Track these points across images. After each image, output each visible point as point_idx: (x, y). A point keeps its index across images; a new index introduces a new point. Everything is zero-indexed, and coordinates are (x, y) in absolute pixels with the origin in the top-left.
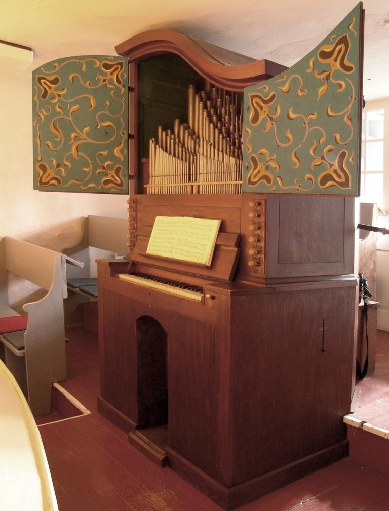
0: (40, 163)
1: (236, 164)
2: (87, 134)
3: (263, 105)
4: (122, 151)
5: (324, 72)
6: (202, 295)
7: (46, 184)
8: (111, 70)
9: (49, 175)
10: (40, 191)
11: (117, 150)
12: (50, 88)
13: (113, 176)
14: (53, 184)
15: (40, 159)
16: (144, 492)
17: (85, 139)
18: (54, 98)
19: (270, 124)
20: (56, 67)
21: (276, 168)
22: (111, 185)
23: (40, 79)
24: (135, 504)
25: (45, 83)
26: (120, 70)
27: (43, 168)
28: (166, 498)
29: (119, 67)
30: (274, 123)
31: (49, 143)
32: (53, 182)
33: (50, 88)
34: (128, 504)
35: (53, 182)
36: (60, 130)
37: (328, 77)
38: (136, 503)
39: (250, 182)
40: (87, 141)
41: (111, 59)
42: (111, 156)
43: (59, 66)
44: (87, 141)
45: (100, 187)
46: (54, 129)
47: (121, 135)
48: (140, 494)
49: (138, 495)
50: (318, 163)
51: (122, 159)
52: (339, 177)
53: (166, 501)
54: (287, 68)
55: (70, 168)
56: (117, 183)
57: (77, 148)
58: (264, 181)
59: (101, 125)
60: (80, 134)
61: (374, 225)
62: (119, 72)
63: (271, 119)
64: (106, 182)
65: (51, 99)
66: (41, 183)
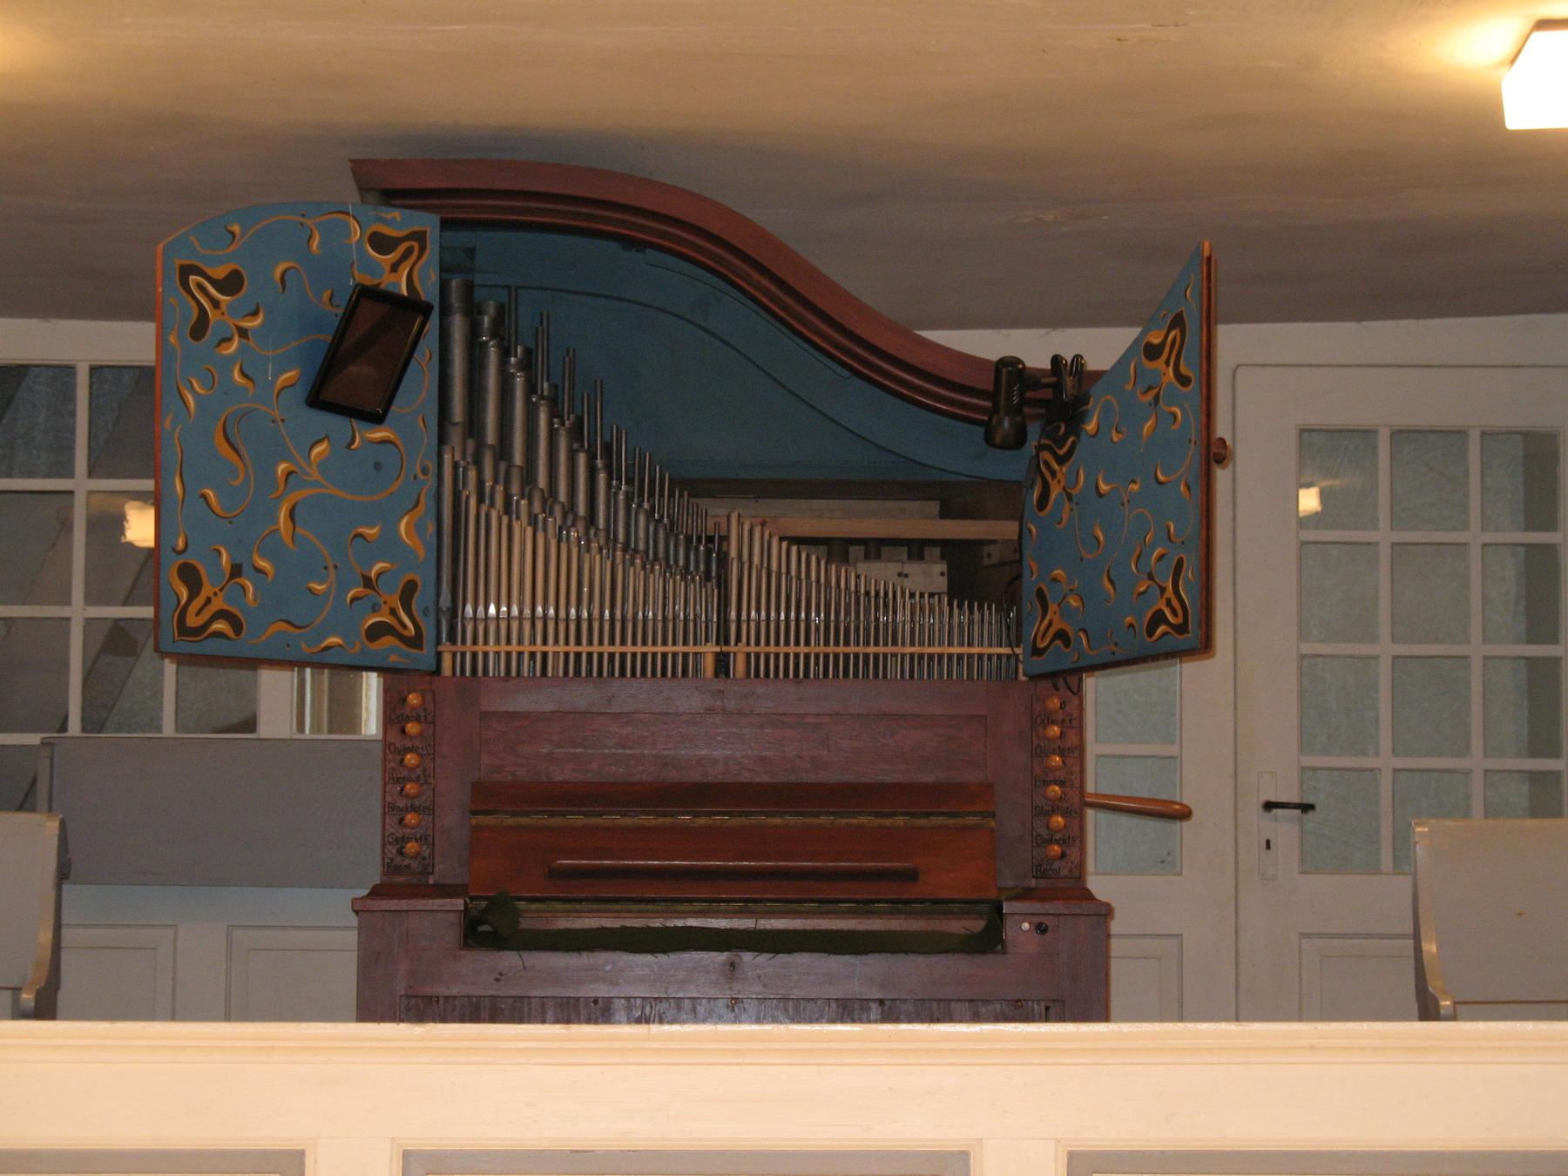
0: (180, 560)
3: (1056, 467)
4: (417, 527)
5: (1150, 388)
8: (392, 257)
9: (208, 601)
13: (393, 612)
14: (219, 634)
15: (181, 544)
18: (230, 339)
20: (233, 234)
21: (1077, 609)
22: (388, 641)
23: (186, 271)
25: (201, 287)
26: (419, 258)
29: (416, 245)
31: (210, 493)
32: (219, 626)
33: (216, 304)
35: (219, 626)
36: (242, 449)
37: (1157, 398)
39: (1037, 652)
43: (243, 233)
45: (357, 648)
51: (422, 553)
54: (1104, 372)
55: (271, 575)
56: (405, 633)
57: (292, 514)
58: (1058, 643)
59: (362, 437)
61: (65, 888)
64: (375, 632)
65: (219, 344)
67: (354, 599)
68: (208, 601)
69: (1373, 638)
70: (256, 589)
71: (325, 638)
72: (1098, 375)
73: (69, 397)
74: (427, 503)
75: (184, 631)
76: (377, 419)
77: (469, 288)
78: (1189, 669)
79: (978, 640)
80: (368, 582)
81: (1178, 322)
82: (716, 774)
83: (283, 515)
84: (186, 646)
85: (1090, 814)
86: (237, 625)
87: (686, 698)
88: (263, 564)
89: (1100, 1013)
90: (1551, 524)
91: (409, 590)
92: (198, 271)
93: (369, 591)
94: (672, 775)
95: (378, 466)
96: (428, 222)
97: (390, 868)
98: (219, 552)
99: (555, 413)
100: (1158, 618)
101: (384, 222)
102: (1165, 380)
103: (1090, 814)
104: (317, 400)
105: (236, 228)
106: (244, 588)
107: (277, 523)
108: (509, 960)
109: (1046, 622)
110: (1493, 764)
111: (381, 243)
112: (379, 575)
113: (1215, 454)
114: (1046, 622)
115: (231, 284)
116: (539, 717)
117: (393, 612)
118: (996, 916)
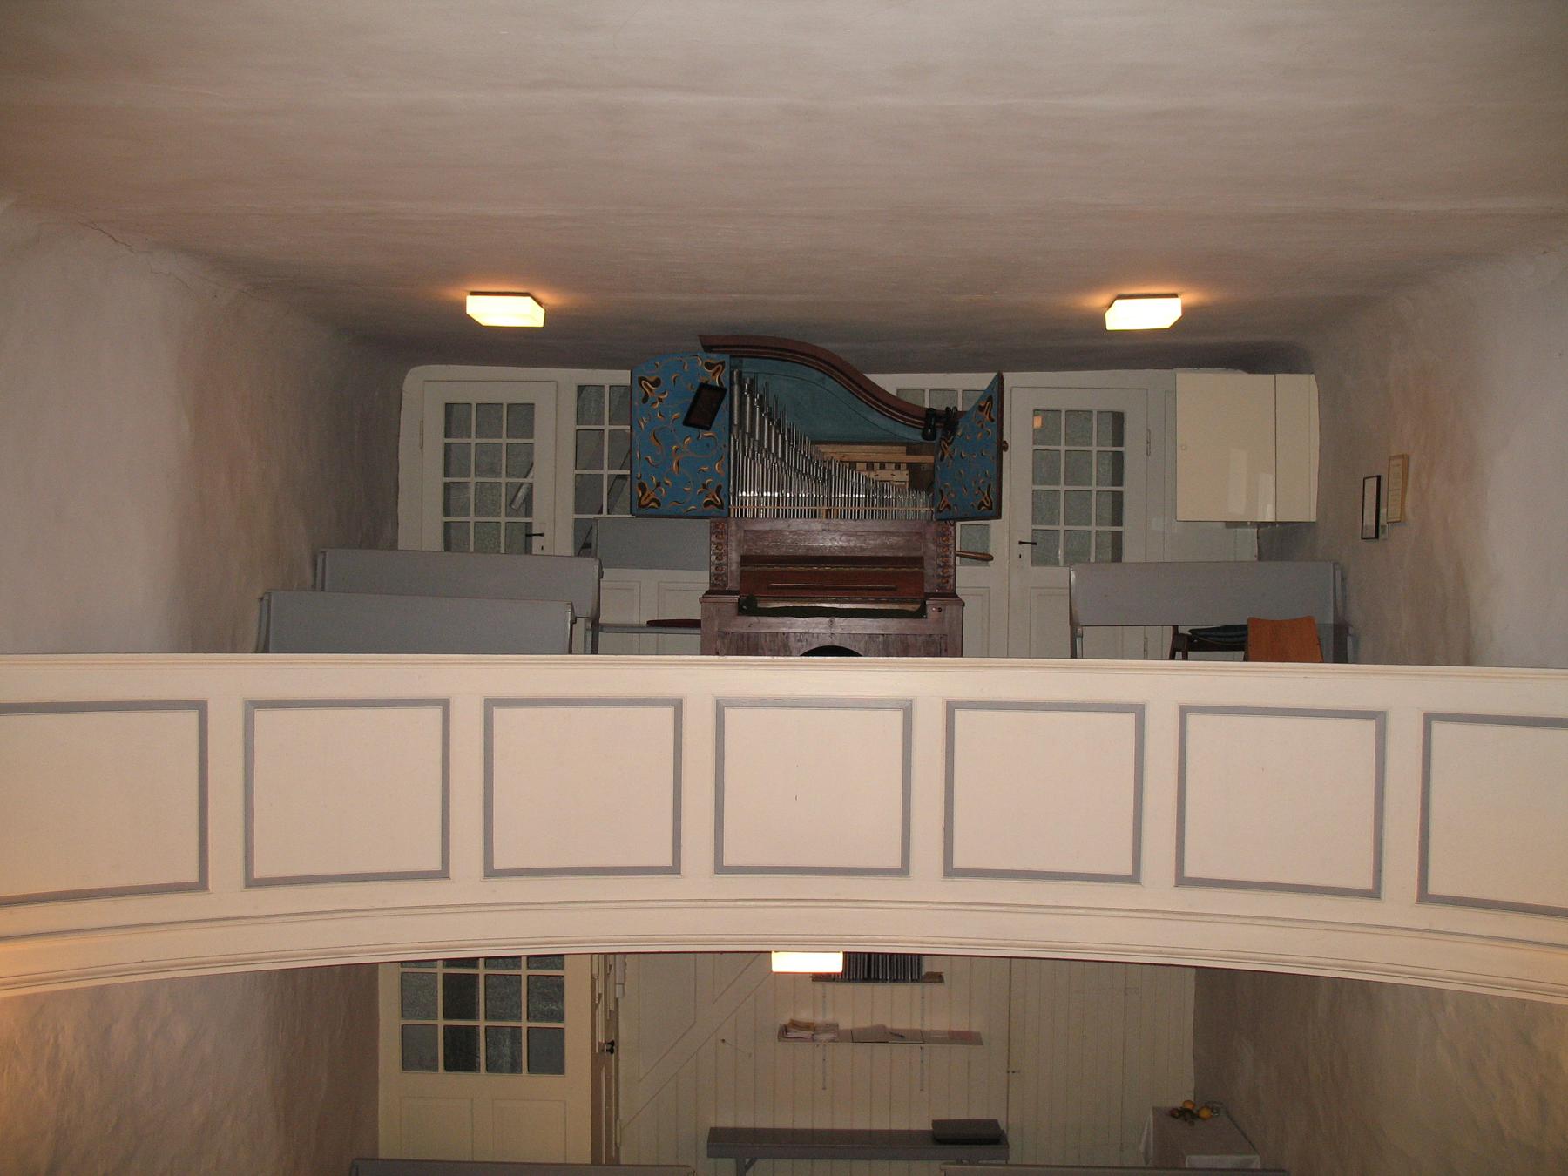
64: (706, 504)
69: (1058, 484)
72: (963, 413)
73: (602, 396)
74: (725, 460)
75: (640, 506)
76: (708, 429)
77: (740, 374)
78: (993, 523)
79: (921, 505)
81: (990, 399)
82: (827, 553)
84: (642, 512)
87: (816, 525)
89: (958, 652)
90: (1121, 444)
91: (719, 488)
94: (811, 553)
96: (725, 358)
97: (712, 584)
99: (770, 420)
100: (982, 504)
104: (686, 423)
108: (754, 619)
110: (1094, 482)
111: (709, 366)
113: (1003, 446)
115: (656, 383)
116: (766, 532)
118: (924, 607)
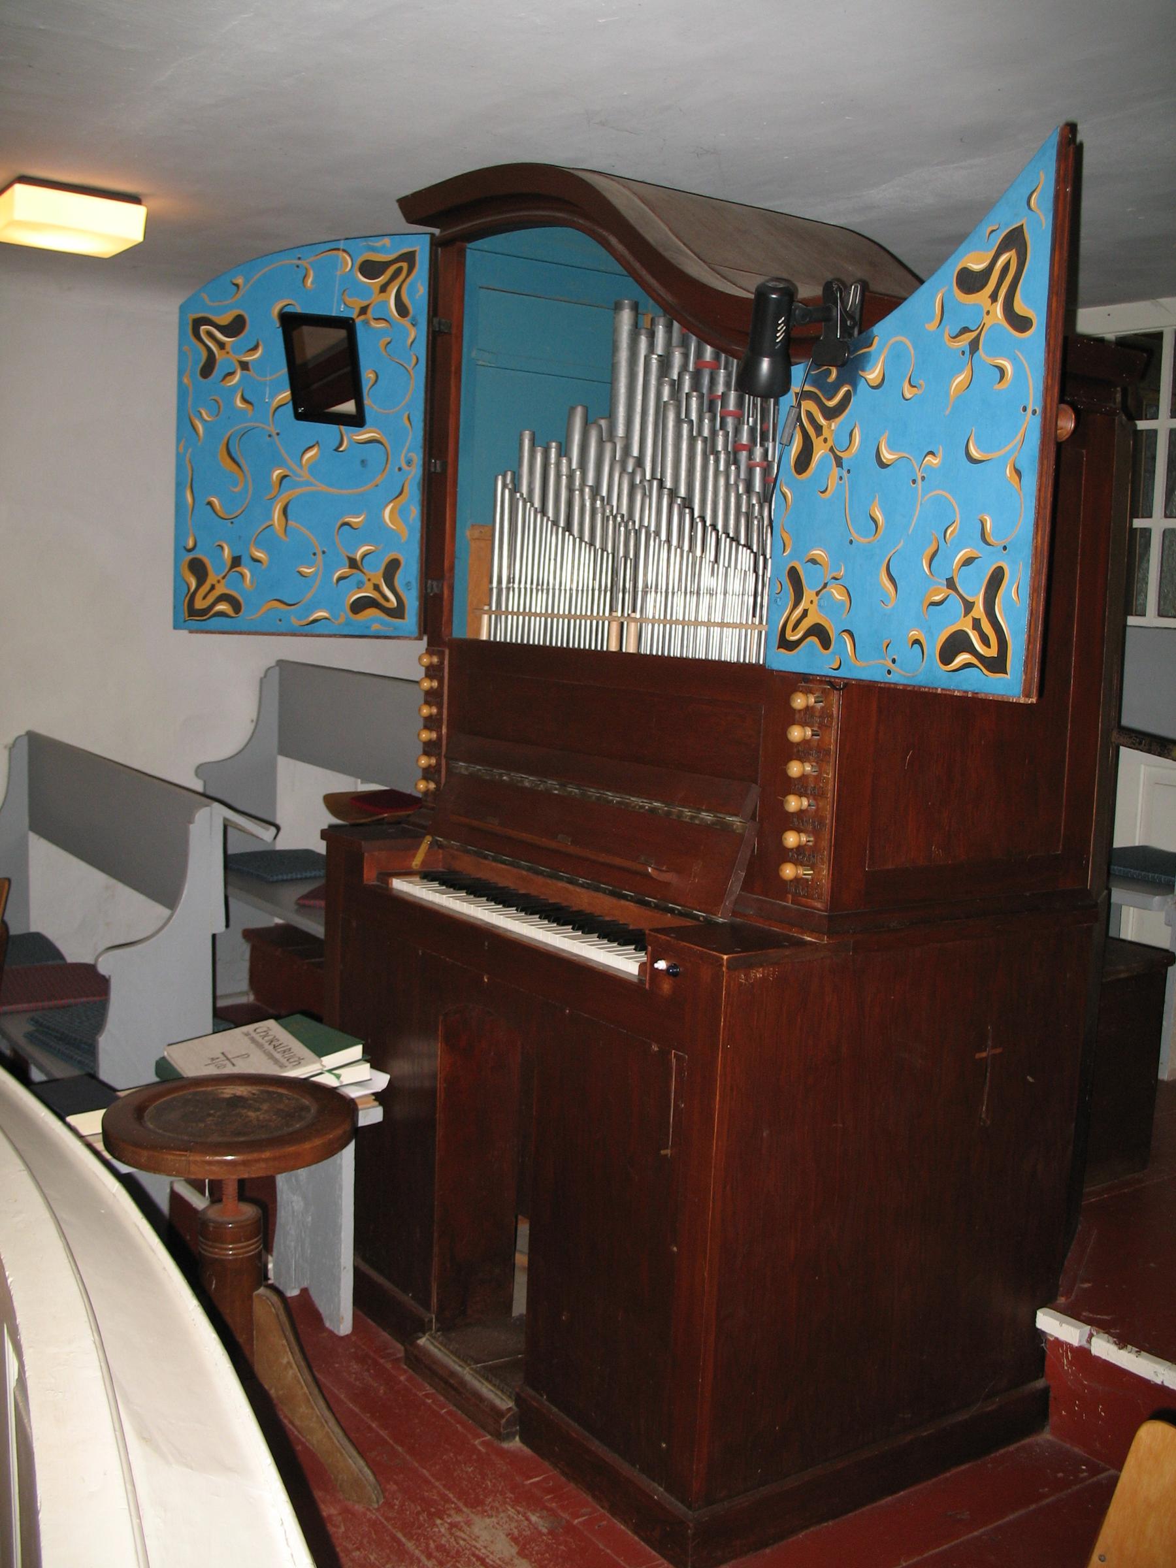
0: (191, 556)
1: (756, 571)
2: (314, 467)
3: (822, 421)
5: (965, 330)
6: (642, 957)
7: (204, 612)
9: (213, 587)
10: (191, 632)
11: (391, 512)
12: (222, 346)
13: (377, 588)
15: (191, 544)
16: (452, 1512)
17: (308, 484)
19: (837, 478)
20: (237, 285)
21: (842, 602)
22: (371, 612)
23: (198, 323)
24: (427, 1545)
25: (210, 335)
27: (198, 568)
28: (516, 1532)
29: (405, 265)
30: (845, 473)
32: (222, 607)
33: (222, 346)
34: (410, 1545)
35: (222, 607)
36: (245, 467)
37: (974, 345)
38: (432, 1545)
40: (314, 488)
41: (384, 246)
42: (375, 529)
44: (314, 488)
45: (342, 620)
46: (229, 461)
47: (404, 466)
48: (442, 1519)
49: (439, 1522)
50: (937, 598)
52: (985, 641)
53: (515, 1540)
58: (813, 640)
60: (295, 467)
62: (404, 281)
63: (839, 462)
64: (359, 606)
66: (193, 612)
67: (340, 579)
68: (213, 587)
70: (252, 575)
71: (313, 613)
80: (353, 564)
83: (277, 514)
85: (1128, 756)
86: (237, 606)
88: (259, 555)
91: (392, 567)
92: (206, 321)
93: (354, 571)
95: (363, 463)
98: (222, 547)
101: (373, 249)
102: (989, 321)
103: (1128, 756)
105: (240, 281)
106: (242, 575)
107: (272, 520)
109: (798, 612)
112: (364, 556)
114: (798, 612)
117: (377, 588)
